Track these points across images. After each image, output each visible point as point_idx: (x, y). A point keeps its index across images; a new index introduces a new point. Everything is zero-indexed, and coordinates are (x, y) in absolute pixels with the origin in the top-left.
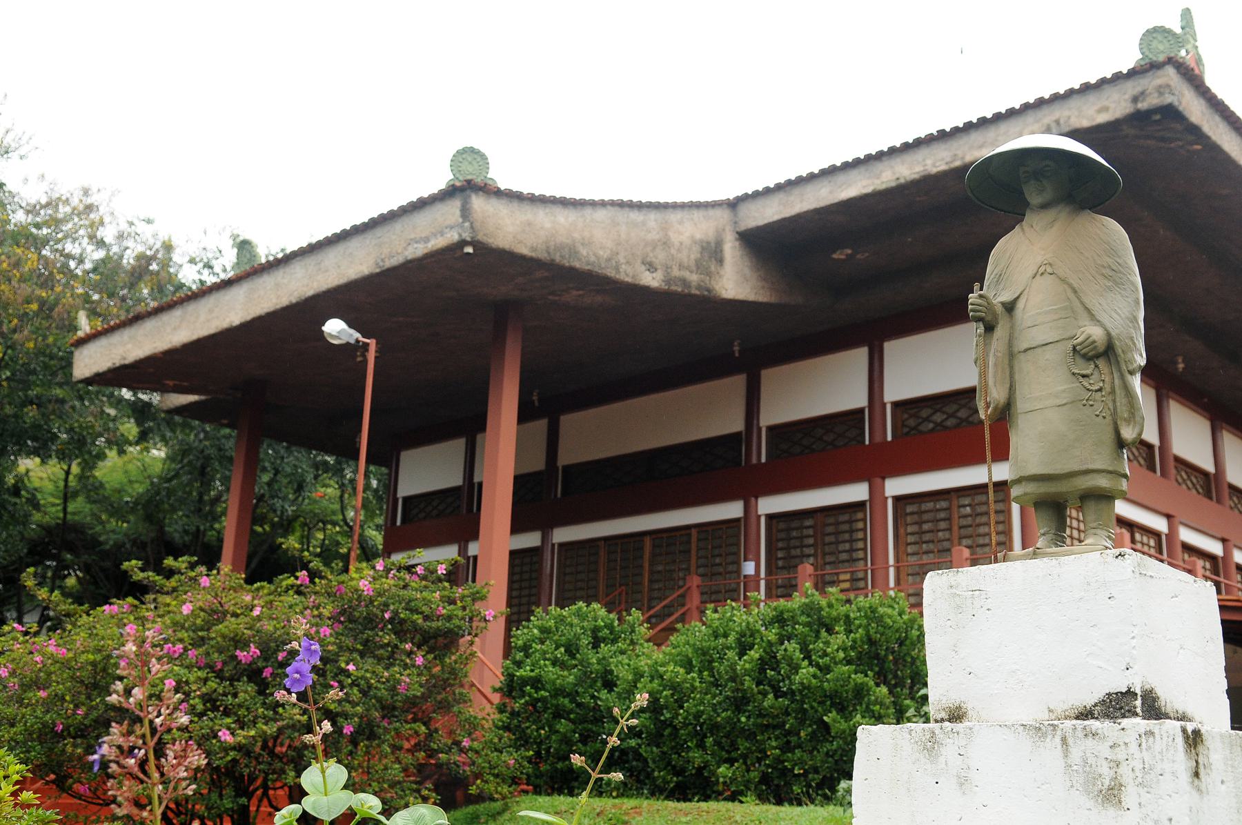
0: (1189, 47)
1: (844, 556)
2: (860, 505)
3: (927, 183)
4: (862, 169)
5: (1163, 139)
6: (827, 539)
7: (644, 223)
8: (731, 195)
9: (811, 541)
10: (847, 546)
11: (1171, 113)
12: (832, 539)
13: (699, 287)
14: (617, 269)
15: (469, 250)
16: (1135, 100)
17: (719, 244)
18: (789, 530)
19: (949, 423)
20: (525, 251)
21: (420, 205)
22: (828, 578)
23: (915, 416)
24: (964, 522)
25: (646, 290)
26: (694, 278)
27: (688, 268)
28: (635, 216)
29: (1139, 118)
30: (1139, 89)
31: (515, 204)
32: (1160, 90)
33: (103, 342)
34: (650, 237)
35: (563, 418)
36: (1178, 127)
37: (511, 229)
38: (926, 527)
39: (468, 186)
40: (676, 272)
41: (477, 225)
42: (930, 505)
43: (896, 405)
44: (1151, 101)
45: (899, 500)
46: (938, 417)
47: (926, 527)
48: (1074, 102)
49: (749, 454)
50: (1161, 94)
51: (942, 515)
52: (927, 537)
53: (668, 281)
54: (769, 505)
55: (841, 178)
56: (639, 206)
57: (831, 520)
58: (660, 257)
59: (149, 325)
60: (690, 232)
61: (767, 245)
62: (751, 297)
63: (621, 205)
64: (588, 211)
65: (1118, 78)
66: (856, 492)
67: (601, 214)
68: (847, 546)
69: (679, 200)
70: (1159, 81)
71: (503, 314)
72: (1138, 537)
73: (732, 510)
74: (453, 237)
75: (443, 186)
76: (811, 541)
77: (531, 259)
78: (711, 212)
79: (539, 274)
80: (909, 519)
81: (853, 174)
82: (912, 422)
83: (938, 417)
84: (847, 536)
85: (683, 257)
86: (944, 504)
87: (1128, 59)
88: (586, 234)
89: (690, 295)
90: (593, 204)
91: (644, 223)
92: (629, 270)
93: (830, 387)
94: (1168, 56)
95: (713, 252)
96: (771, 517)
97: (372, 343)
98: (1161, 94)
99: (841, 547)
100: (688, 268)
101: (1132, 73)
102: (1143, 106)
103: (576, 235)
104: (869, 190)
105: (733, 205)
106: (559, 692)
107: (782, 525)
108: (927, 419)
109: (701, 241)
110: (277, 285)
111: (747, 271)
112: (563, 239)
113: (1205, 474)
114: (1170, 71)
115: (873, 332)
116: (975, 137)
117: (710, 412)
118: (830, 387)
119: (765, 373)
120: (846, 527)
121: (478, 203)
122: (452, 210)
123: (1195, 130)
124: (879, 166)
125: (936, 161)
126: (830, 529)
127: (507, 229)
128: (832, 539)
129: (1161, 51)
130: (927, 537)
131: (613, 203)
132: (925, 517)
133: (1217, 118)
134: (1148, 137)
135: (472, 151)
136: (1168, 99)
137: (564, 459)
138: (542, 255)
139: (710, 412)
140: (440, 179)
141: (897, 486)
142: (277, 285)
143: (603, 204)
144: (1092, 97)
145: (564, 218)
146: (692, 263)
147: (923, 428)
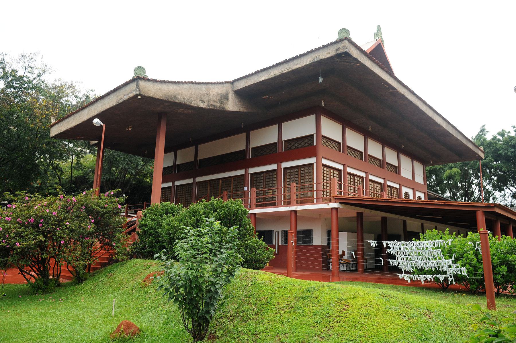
0: (379, 37)
1: (271, 185)
2: (274, 171)
3: (283, 76)
4: (266, 72)
5: (348, 62)
6: (267, 180)
7: (200, 89)
8: (232, 79)
9: (262, 181)
10: (272, 182)
11: (347, 54)
12: (268, 180)
13: (220, 107)
14: (191, 102)
15: (139, 97)
16: (337, 50)
17: (227, 94)
18: (257, 178)
19: (299, 147)
20: (158, 97)
21: (126, 84)
22: (266, 191)
23: (290, 144)
24: (302, 175)
25: (202, 108)
26: (218, 105)
27: (216, 102)
28: (197, 86)
29: (338, 55)
30: (338, 47)
31: (155, 83)
32: (343, 47)
33: (57, 126)
34: (203, 93)
35: (199, 146)
36: (351, 59)
37: (153, 91)
38: (292, 177)
39: (139, 77)
40: (212, 103)
41: (141, 90)
42: (293, 170)
43: (285, 141)
44: (341, 51)
45: (285, 169)
46: (296, 145)
47: (292, 177)
48: (321, 51)
49: (246, 156)
50: (343, 48)
51: (297, 173)
52: (292, 179)
53: (209, 106)
54: (252, 170)
55: (260, 74)
56: (199, 83)
57: (268, 175)
58: (206, 98)
59: (67, 121)
60: (216, 91)
61: (243, 94)
62: (238, 110)
63: (192, 83)
64: (181, 85)
65: (332, 44)
66: (274, 167)
67: (185, 86)
68: (272, 182)
69: (213, 81)
70: (343, 45)
71: (160, 115)
72: (356, 178)
73: (242, 172)
74: (134, 93)
75: (131, 78)
76: (262, 181)
77: (161, 100)
78: (224, 85)
79: (167, 104)
80: (288, 174)
81: (264, 73)
82: (289, 146)
83: (303, 144)
84: (272, 179)
85: (214, 98)
86: (297, 170)
87: (335, 38)
88: (180, 92)
89: (217, 110)
90: (182, 83)
91: (200, 89)
92: (195, 102)
93: (267, 136)
94: (344, 37)
95: (225, 97)
96: (252, 174)
97: (104, 125)
98: (343, 48)
99: (270, 183)
100: (216, 102)
101: (336, 42)
102: (339, 52)
103: (176, 92)
104: (267, 78)
105: (232, 83)
106: (151, 228)
107: (255, 176)
108: (293, 145)
109: (221, 94)
110: (94, 109)
111: (237, 103)
112: (171, 93)
113: (380, 160)
114: (346, 41)
115: (279, 120)
116: (295, 62)
117: (236, 144)
118: (267, 136)
119: (251, 132)
120: (272, 177)
121: (141, 83)
122: (133, 86)
123: (356, 59)
124: (270, 71)
125: (285, 69)
126: (267, 177)
127: (151, 91)
128: (268, 180)
129: (344, 35)
130: (292, 179)
131: (189, 83)
132: (292, 174)
133: (364, 56)
134: (343, 62)
135: (140, 67)
136: (345, 50)
137: (199, 158)
138: (165, 99)
139: (236, 144)
140: (130, 76)
141: (285, 165)
142: (94, 109)
143: (186, 83)
144: (325, 50)
145: (172, 87)
146: (217, 100)
147: (299, 147)
